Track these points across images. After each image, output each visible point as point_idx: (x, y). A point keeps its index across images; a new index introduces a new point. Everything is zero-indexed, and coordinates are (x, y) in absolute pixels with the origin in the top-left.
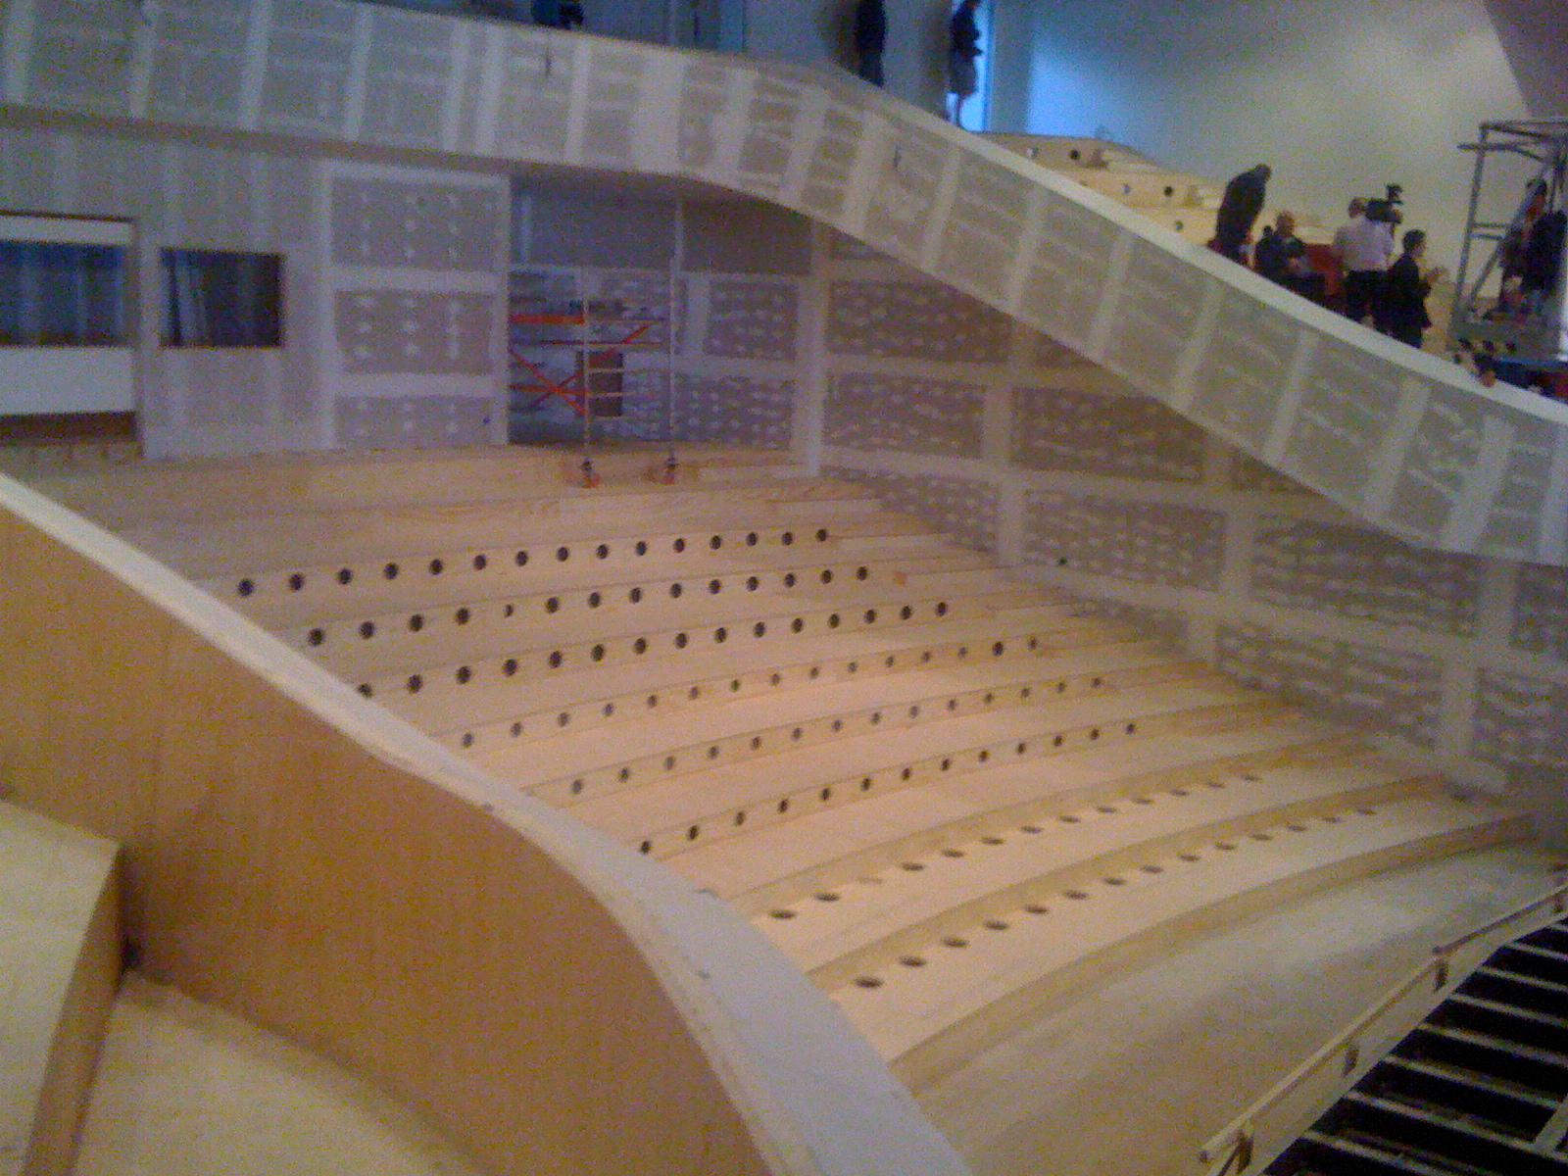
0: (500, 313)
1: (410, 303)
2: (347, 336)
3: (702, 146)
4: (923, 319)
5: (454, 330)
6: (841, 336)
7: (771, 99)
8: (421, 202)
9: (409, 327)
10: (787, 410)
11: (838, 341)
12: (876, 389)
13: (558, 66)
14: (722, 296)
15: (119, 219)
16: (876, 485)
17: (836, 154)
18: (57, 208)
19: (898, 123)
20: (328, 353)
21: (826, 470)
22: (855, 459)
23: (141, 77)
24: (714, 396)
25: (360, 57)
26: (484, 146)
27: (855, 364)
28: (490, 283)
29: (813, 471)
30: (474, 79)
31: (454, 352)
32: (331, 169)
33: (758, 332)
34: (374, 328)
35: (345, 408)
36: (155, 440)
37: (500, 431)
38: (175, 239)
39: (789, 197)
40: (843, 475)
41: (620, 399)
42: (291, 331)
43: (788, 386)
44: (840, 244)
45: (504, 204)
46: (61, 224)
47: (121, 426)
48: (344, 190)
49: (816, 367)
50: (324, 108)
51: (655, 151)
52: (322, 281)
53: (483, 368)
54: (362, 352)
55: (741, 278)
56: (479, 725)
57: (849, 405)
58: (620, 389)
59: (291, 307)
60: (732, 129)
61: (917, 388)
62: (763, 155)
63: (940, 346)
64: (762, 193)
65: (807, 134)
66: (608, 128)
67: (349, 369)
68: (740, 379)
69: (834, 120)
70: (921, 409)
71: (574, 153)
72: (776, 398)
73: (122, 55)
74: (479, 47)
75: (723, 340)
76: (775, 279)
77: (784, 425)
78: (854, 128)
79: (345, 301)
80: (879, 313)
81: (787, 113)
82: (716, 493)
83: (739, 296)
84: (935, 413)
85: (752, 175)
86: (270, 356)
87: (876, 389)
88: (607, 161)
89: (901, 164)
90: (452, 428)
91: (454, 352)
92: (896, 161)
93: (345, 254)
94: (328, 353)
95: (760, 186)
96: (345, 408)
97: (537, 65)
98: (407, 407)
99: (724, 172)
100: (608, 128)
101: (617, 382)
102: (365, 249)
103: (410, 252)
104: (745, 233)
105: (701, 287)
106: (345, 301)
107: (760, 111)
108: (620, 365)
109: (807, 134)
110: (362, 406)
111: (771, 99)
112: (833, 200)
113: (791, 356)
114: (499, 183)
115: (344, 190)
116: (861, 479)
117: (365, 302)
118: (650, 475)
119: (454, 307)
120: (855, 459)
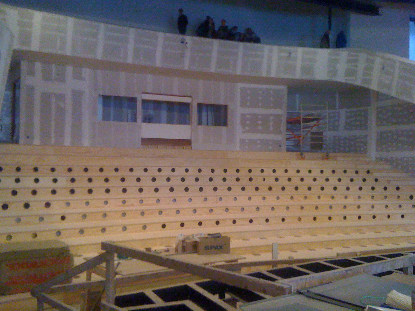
0: (284, 120)
1: (260, 117)
2: (243, 123)
3: (334, 72)
4: (401, 114)
5: (271, 123)
6: (380, 121)
7: (352, 58)
8: (263, 93)
9: (259, 122)
10: (366, 143)
11: (379, 123)
12: (389, 134)
13: (293, 55)
14: (348, 114)
15: (188, 97)
16: (387, 161)
17: (369, 69)
18: (175, 93)
19: (383, 58)
20: (238, 127)
21: (377, 159)
22: (384, 155)
23: (187, 61)
24: (347, 141)
25: (240, 56)
26: (273, 75)
27: (384, 128)
28: (282, 112)
29: (373, 159)
30: (270, 58)
31: (271, 129)
32: (240, 85)
33: (358, 123)
34: (251, 123)
35: (242, 141)
36: (193, 145)
37: (284, 148)
38: (201, 101)
39: (358, 83)
40: (381, 159)
41: (322, 144)
42: (229, 123)
43: (366, 137)
44: (378, 95)
45: (285, 93)
46: (176, 97)
47: (187, 143)
48: (243, 90)
49: (373, 130)
50: (231, 67)
51: (320, 74)
52: (237, 111)
53: (280, 132)
54: (247, 128)
55: (354, 109)
56: (227, 176)
57: (384, 141)
58: (322, 141)
59: (229, 118)
60: (342, 67)
61: (401, 133)
62: (351, 72)
63: (406, 120)
64: (350, 82)
65: (362, 65)
66: (308, 69)
67: (244, 132)
68: (353, 136)
69: (368, 60)
70: (401, 139)
71: (298, 75)
72: (363, 140)
73: (182, 56)
74: (271, 51)
75: (349, 126)
76: (362, 108)
77: (365, 147)
78: (373, 62)
79: (243, 116)
80: (390, 114)
81: (356, 61)
82: (340, 162)
83: (353, 114)
84: (405, 139)
85: (347, 78)
86: (224, 128)
87: (389, 134)
88: (307, 77)
89: (385, 69)
90: (271, 147)
91: (271, 129)
92: (383, 68)
93: (243, 104)
94: (238, 127)
95: (351, 81)
96: (242, 141)
97: (287, 55)
98: (259, 142)
99: (340, 78)
100: (308, 69)
101: (321, 139)
102: (248, 104)
103: (260, 104)
104: (354, 96)
105: (343, 113)
106: (243, 116)
107: (349, 61)
108: (322, 135)
109: (362, 65)
110: (247, 141)
111: (352, 58)
112: (369, 82)
113: (366, 128)
114: (284, 88)
115: (243, 90)
116: (387, 161)
117: (248, 116)
118: (323, 159)
119: (272, 118)
120: (384, 155)
